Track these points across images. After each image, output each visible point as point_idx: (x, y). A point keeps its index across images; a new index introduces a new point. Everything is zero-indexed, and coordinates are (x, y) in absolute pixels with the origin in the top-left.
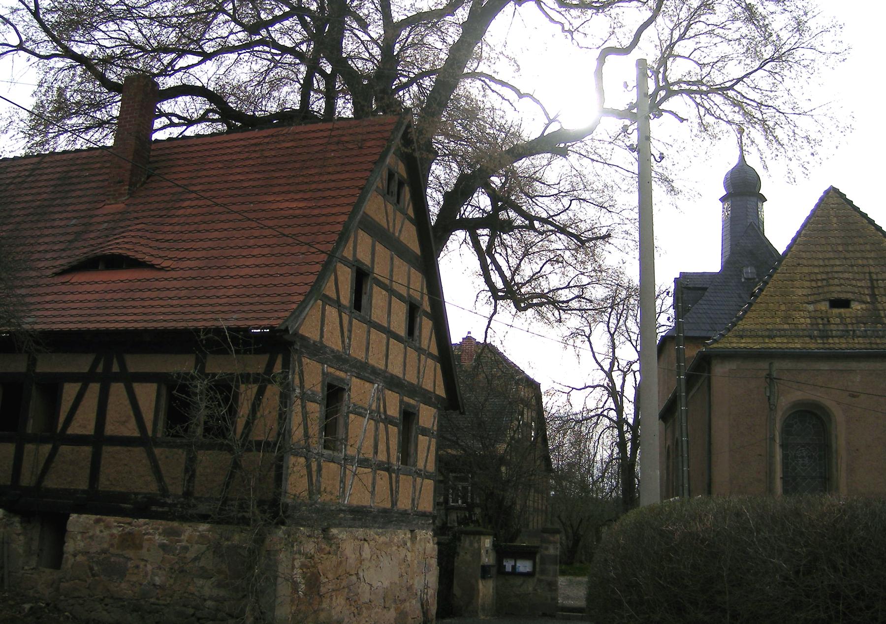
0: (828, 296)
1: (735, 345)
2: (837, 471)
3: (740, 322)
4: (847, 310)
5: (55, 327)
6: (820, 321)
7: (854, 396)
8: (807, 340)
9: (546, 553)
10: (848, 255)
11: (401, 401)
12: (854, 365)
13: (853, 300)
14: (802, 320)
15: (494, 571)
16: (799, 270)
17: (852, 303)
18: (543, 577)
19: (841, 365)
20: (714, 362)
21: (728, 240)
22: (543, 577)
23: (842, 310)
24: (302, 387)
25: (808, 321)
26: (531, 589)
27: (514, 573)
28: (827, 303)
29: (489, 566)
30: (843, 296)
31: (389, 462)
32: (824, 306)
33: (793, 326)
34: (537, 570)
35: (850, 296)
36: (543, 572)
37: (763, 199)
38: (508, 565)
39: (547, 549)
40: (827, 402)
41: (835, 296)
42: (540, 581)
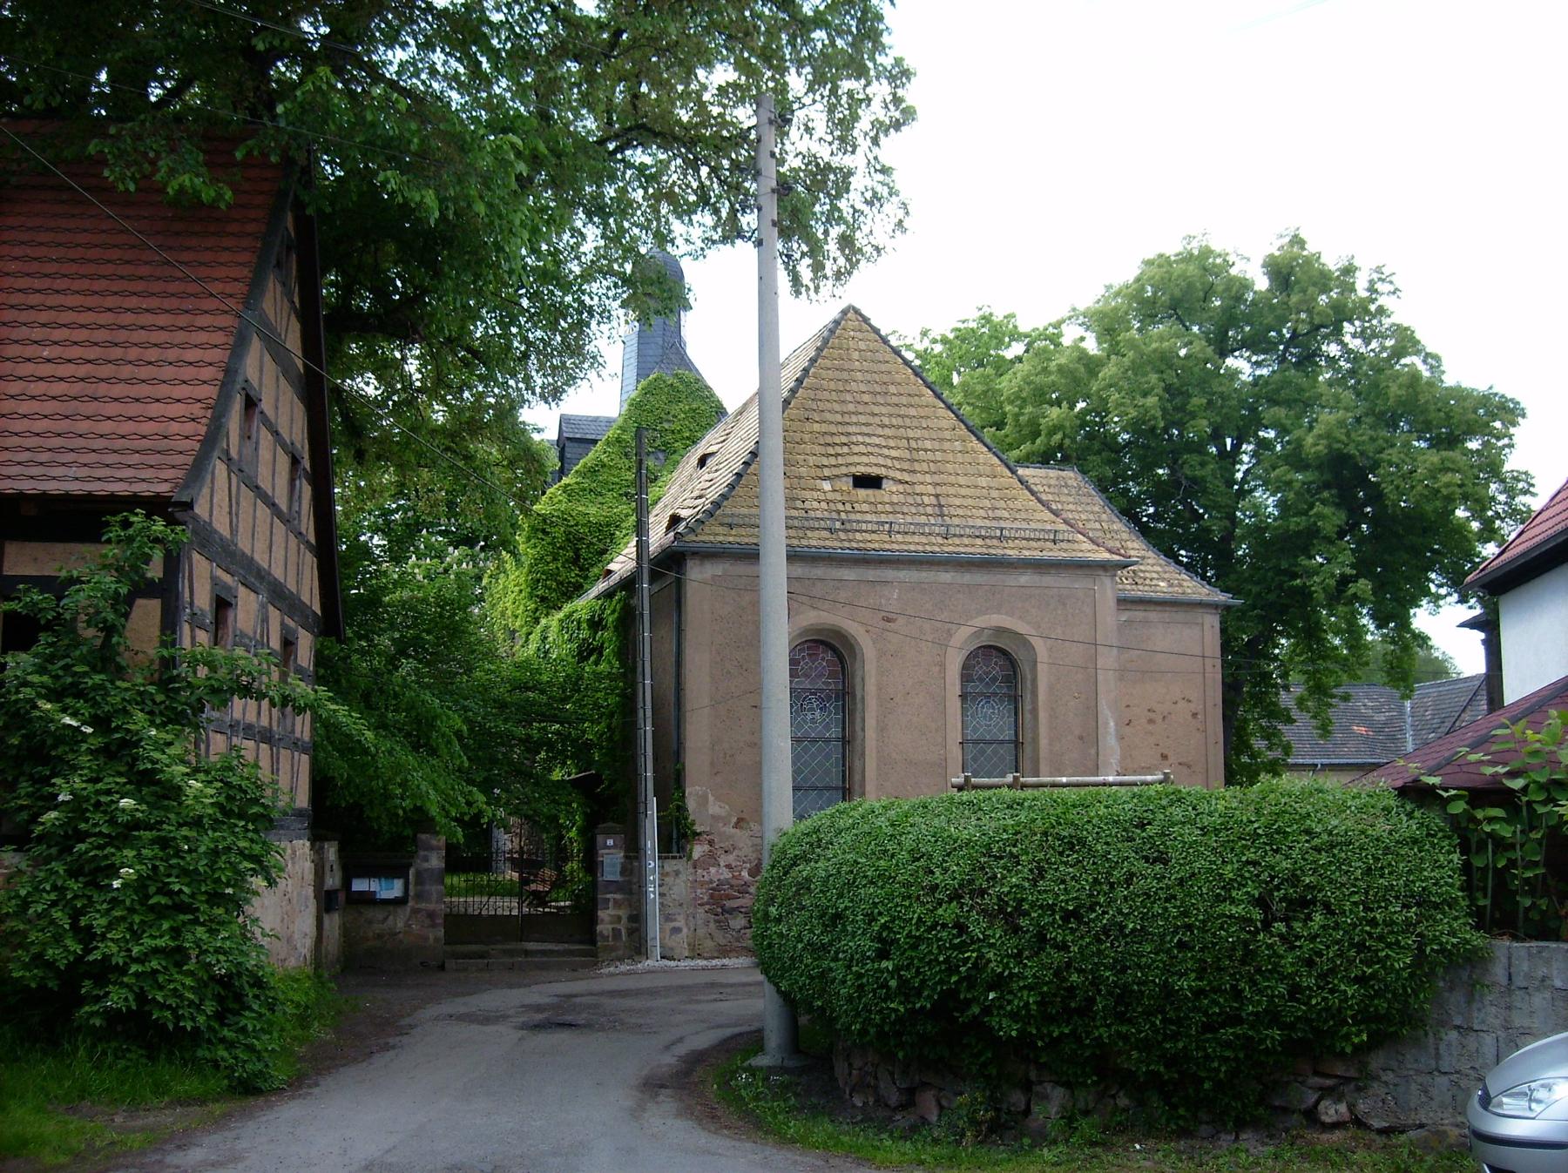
0: (853, 470)
1: (721, 538)
2: (863, 729)
3: (725, 503)
4: (877, 492)
5: (52, 487)
6: (841, 507)
7: (889, 620)
8: (825, 534)
9: (426, 865)
10: (876, 410)
11: (282, 623)
12: (890, 574)
13: (886, 477)
14: (815, 504)
15: (342, 897)
16: (808, 426)
17: (884, 481)
18: (423, 906)
19: (871, 574)
20: (690, 563)
21: (631, 367)
22: (423, 906)
23: (870, 492)
24: (192, 604)
25: (824, 505)
26: (400, 924)
27: (368, 899)
28: (851, 480)
29: (335, 891)
30: (874, 471)
31: (271, 730)
32: (846, 484)
33: (802, 513)
34: (411, 893)
35: (882, 472)
36: (419, 896)
37: (688, 307)
38: (359, 885)
39: (426, 859)
40: (853, 628)
41: (861, 470)
42: (415, 911)
